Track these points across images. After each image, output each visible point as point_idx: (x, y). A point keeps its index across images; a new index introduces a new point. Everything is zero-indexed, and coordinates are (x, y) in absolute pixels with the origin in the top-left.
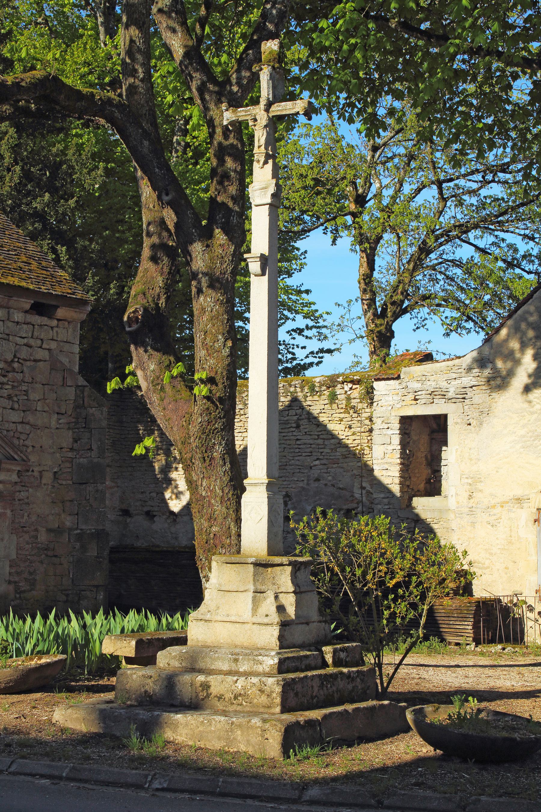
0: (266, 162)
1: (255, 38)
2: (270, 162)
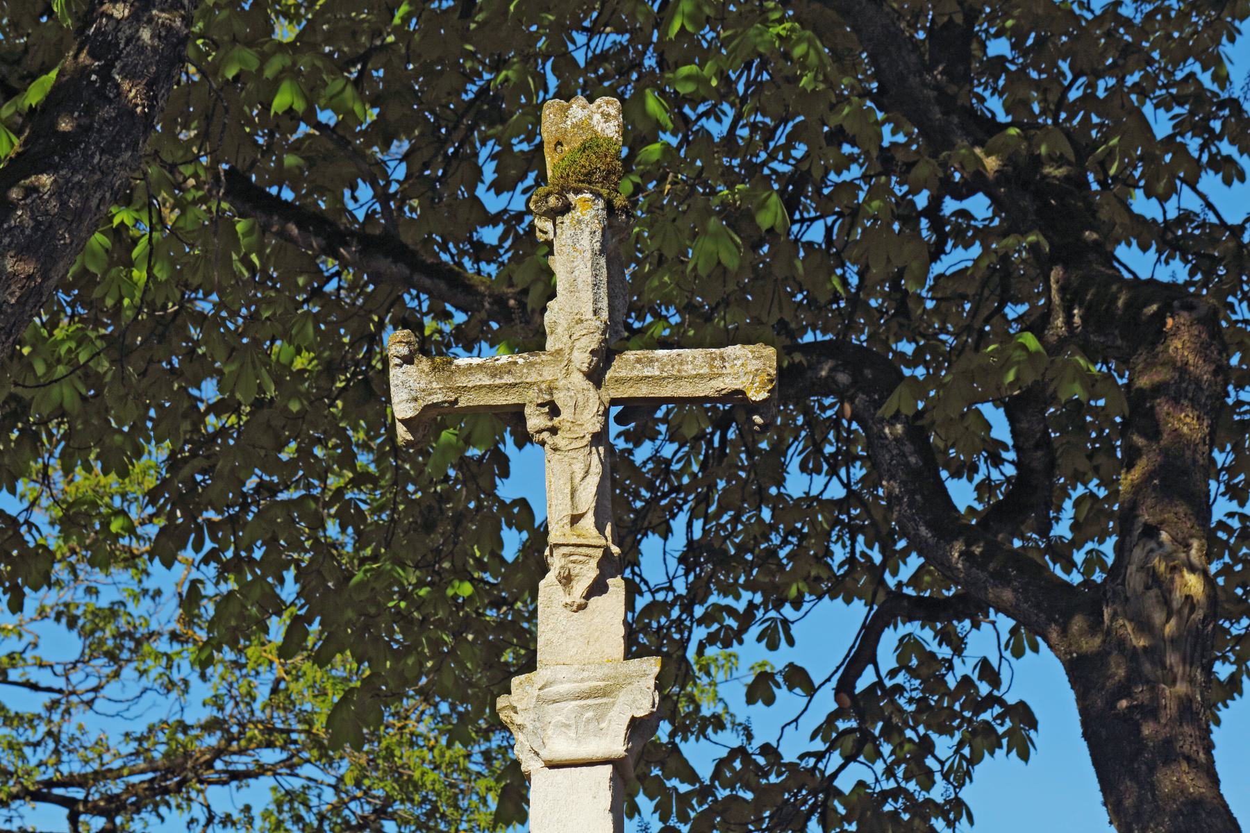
0: (598, 588)
1: (65, 126)
2: (616, 585)
